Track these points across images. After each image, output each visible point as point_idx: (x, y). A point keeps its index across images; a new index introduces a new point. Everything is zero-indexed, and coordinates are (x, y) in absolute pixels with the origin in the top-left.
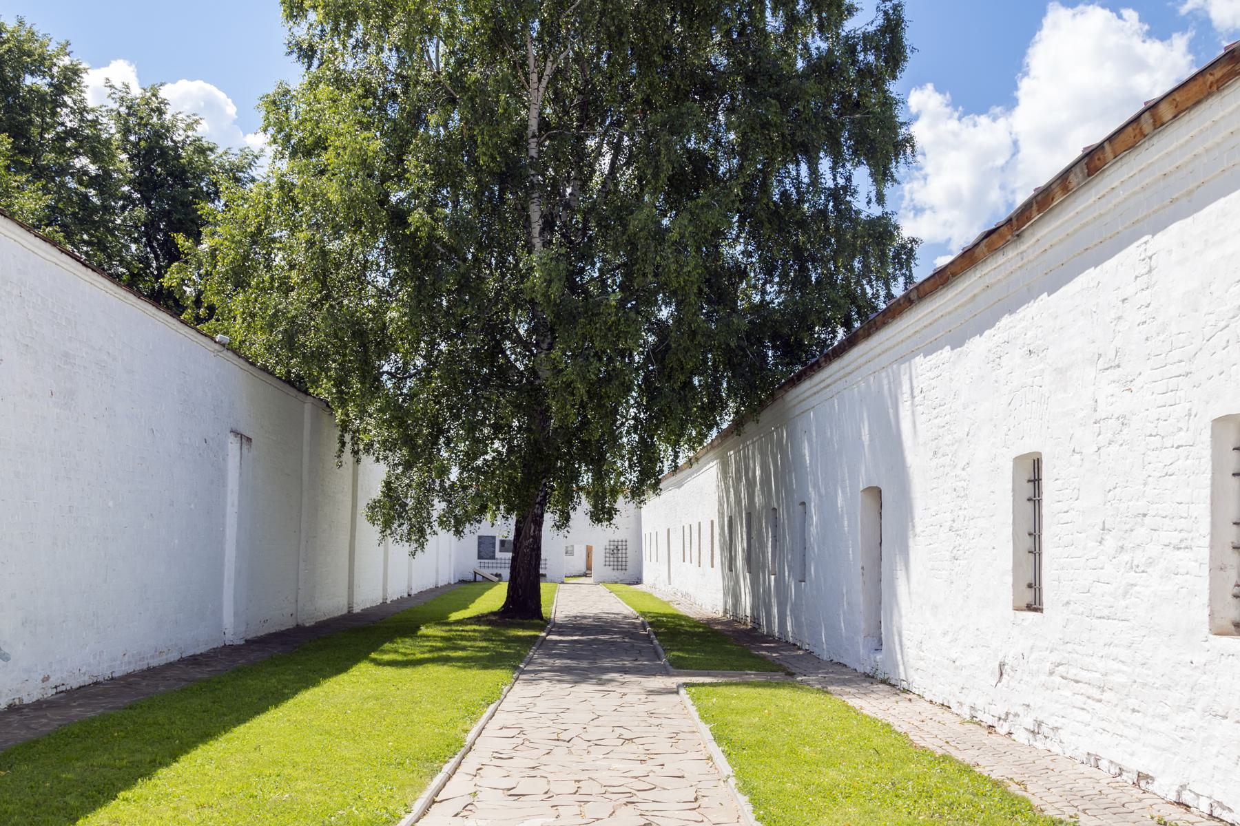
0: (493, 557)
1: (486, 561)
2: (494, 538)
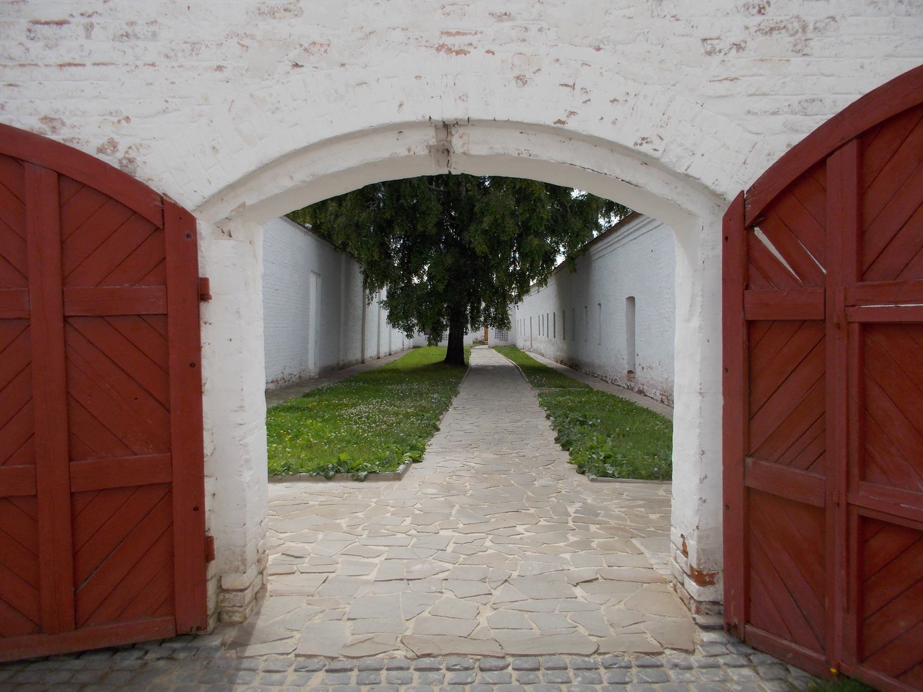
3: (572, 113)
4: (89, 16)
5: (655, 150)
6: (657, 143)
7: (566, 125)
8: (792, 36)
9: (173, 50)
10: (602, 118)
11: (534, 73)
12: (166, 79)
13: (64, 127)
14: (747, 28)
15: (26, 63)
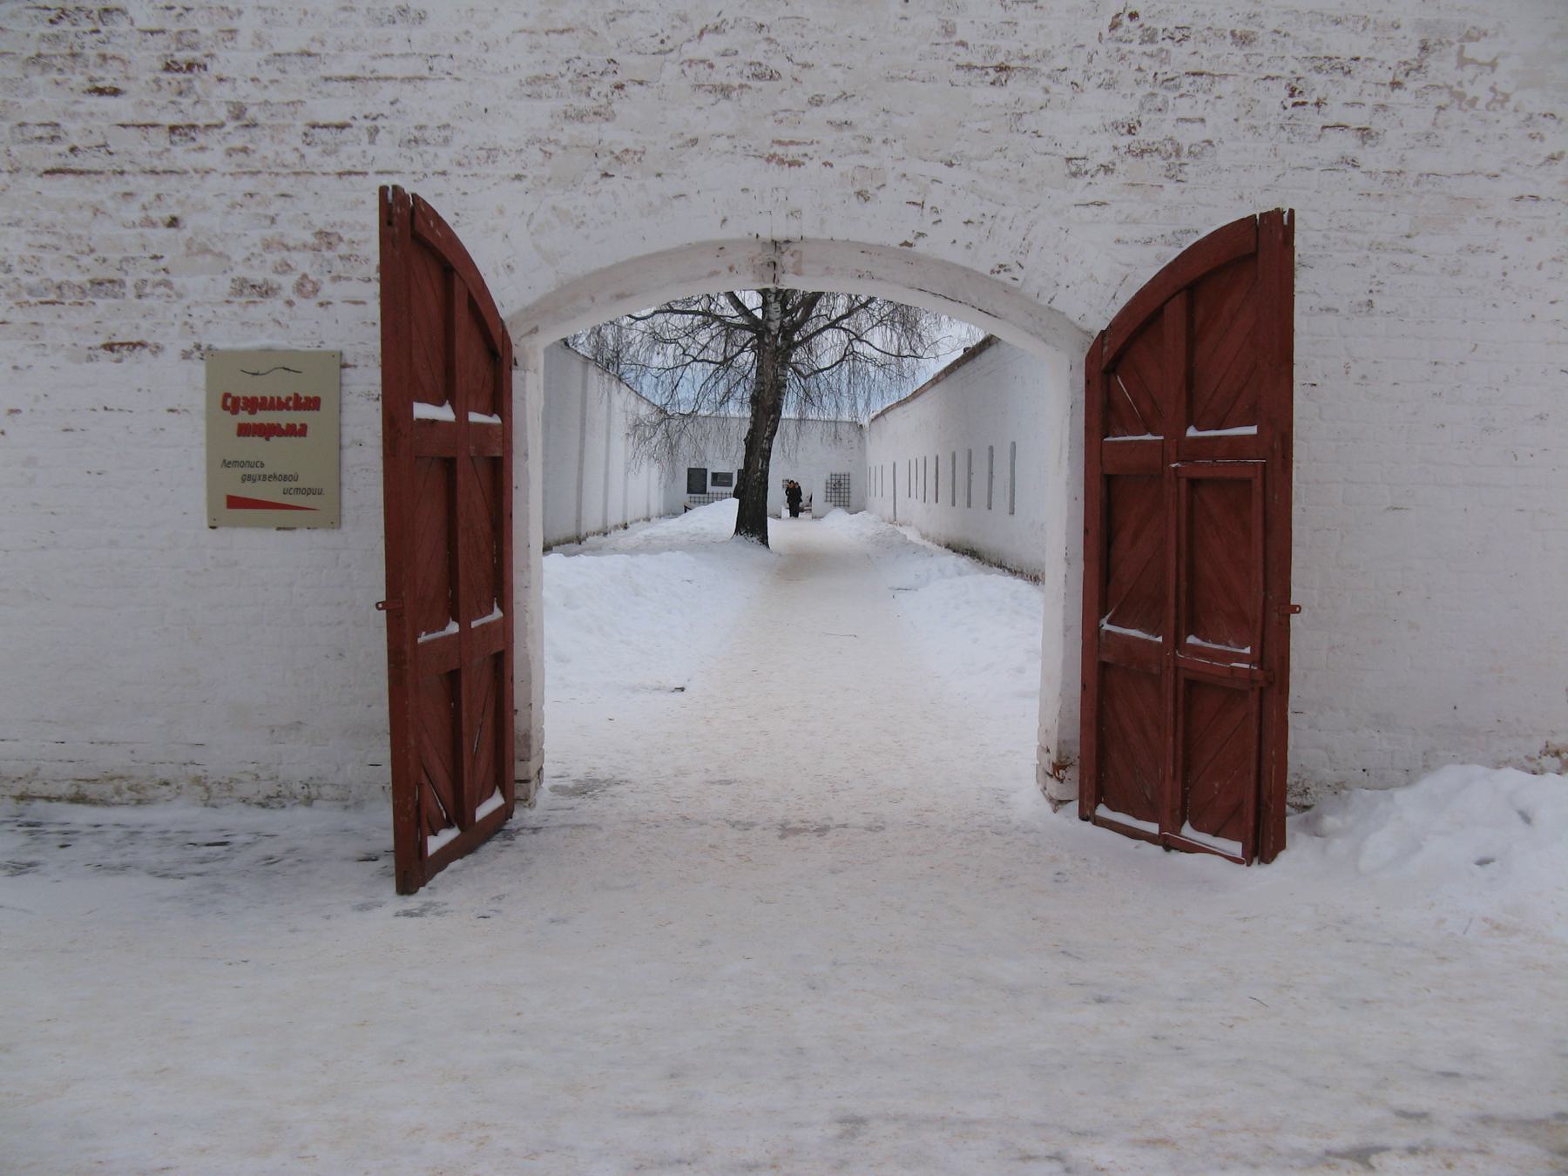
0: (704, 491)
1: (698, 495)
2: (706, 470)
3: (921, 235)
4: (374, 119)
5: (1014, 279)
6: (1017, 273)
7: (913, 248)
8: (1165, 159)
9: (467, 157)
10: (954, 242)
11: (878, 188)
12: (458, 189)
13: (342, 243)
14: (1115, 148)
15: (301, 170)
